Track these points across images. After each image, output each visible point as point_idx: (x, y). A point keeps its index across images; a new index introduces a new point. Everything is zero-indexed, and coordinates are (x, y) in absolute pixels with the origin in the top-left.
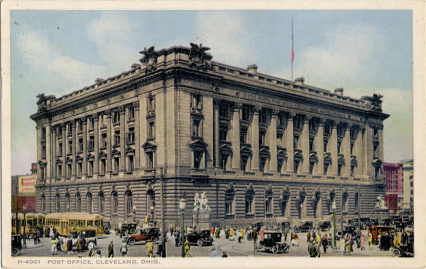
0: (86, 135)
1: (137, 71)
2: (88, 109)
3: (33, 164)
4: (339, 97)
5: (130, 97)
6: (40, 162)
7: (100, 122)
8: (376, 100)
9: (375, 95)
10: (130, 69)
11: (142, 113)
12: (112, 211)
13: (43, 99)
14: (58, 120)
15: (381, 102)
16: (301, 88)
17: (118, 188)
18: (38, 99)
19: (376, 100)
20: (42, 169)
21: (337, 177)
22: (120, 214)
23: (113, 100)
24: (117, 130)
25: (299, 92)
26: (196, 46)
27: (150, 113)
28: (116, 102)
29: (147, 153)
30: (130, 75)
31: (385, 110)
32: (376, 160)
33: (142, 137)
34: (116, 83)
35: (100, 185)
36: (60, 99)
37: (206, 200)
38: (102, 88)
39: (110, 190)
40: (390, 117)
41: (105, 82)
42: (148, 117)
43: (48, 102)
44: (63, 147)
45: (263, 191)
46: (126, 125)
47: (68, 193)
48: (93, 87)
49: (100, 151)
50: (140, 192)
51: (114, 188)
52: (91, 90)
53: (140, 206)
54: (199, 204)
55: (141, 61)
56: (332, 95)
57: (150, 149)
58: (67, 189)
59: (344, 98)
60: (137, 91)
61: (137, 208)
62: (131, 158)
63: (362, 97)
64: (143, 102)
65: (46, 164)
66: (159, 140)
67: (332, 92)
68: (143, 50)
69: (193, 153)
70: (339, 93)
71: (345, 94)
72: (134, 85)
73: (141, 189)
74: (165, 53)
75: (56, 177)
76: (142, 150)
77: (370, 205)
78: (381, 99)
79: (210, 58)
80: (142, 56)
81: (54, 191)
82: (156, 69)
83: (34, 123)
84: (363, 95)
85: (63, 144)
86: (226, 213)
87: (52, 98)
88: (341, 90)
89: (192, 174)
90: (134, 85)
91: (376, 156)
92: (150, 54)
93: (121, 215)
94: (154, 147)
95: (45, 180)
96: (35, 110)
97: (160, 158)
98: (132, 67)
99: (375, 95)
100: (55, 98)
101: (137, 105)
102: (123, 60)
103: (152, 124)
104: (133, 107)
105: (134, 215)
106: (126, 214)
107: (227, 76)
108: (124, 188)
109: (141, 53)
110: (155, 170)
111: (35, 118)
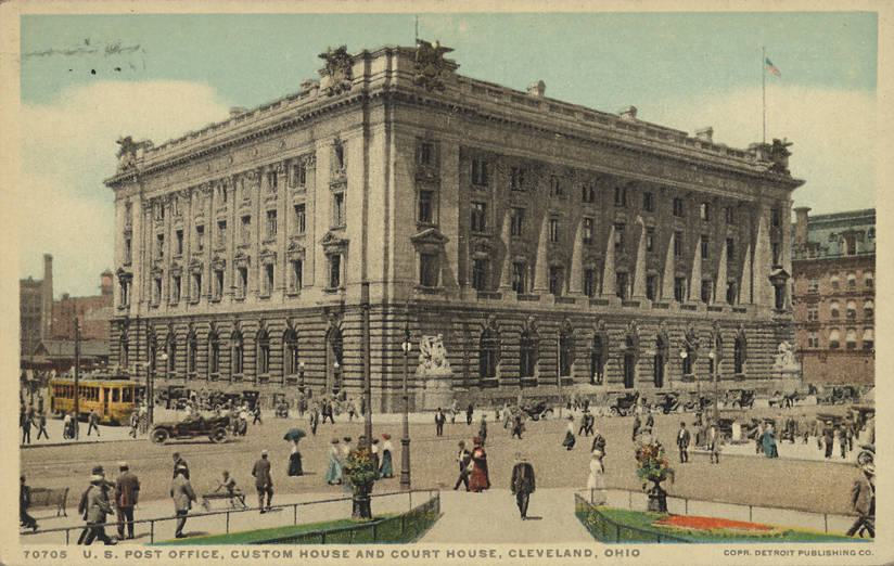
0: (170, 228)
1: (313, 93)
2: (288, 146)
3: (107, 275)
4: (705, 145)
5: (296, 143)
6: (121, 271)
7: (238, 193)
8: (778, 151)
9: (776, 142)
10: (296, 88)
11: (322, 174)
12: (285, 370)
13: (128, 145)
14: (158, 188)
15: (787, 154)
16: (631, 127)
17: (270, 325)
18: (119, 147)
19: (778, 151)
20: (123, 284)
21: (676, 304)
22: (273, 376)
23: (215, 164)
24: (245, 214)
25: (628, 137)
26: (429, 45)
27: (337, 176)
28: (271, 152)
29: (328, 255)
30: (299, 102)
31: (795, 174)
32: (779, 270)
33: (321, 219)
34: (178, 150)
35: (189, 321)
36: (164, 147)
37: (443, 350)
38: (245, 126)
39: (205, 330)
40: (804, 186)
41: (250, 115)
42: (334, 186)
43: (140, 153)
44: (185, 241)
45: (478, 331)
46: (215, 217)
47: (238, 332)
48: (226, 123)
49: (236, 250)
50: (313, 333)
51: (213, 327)
52: (179, 146)
53: (313, 360)
54: (429, 357)
55: (323, 73)
56: (691, 141)
57: (336, 253)
58: (170, 326)
59: (716, 148)
60: (312, 133)
61: (306, 364)
62: (298, 265)
63: (751, 145)
64: (324, 152)
65: (130, 276)
66: (353, 232)
67: (692, 135)
68: (325, 51)
69: (418, 255)
70: (704, 138)
71: (716, 140)
72: (308, 119)
73: (315, 326)
74: (367, 57)
75: (188, 298)
76: (319, 248)
77: (313, 360)
78: (789, 149)
79: (453, 66)
80: (323, 63)
81: (185, 328)
82: (350, 89)
83: (111, 193)
84: (752, 141)
85: (166, 236)
86: (522, 375)
87: (145, 145)
88: (710, 132)
89: (416, 297)
90: (308, 119)
91: (779, 264)
92: (339, 60)
93: (276, 379)
94: (344, 244)
95: (129, 307)
96: (112, 166)
97: (352, 269)
98: (231, 113)
99: (776, 142)
100: (152, 144)
101: (312, 155)
102: (293, 71)
103: (339, 198)
104: (299, 170)
105: (299, 380)
106: (189, 373)
107: (489, 104)
108: (283, 325)
109: (323, 56)
110: (343, 289)
111: (115, 184)
